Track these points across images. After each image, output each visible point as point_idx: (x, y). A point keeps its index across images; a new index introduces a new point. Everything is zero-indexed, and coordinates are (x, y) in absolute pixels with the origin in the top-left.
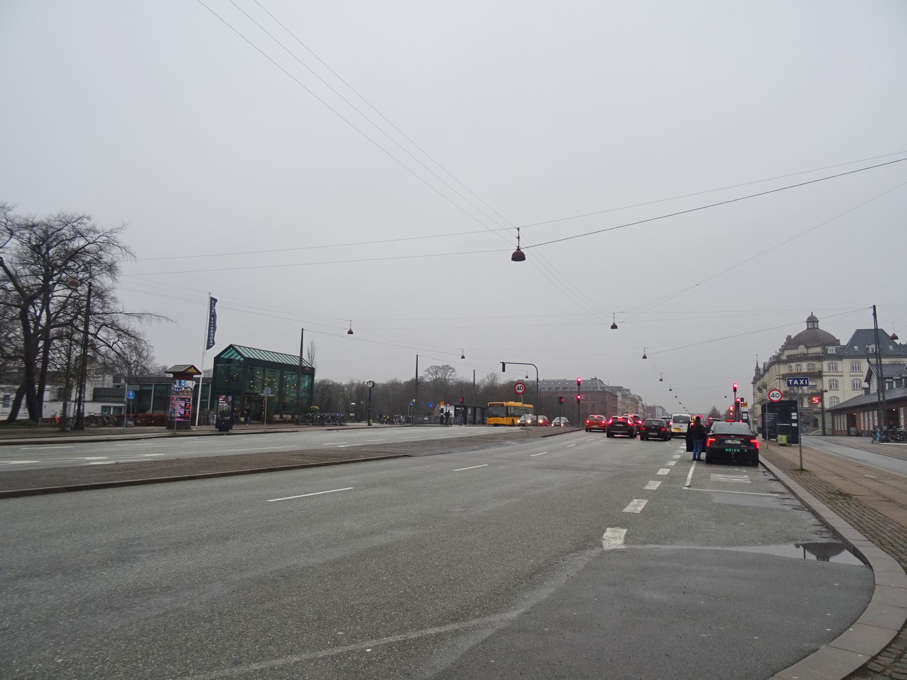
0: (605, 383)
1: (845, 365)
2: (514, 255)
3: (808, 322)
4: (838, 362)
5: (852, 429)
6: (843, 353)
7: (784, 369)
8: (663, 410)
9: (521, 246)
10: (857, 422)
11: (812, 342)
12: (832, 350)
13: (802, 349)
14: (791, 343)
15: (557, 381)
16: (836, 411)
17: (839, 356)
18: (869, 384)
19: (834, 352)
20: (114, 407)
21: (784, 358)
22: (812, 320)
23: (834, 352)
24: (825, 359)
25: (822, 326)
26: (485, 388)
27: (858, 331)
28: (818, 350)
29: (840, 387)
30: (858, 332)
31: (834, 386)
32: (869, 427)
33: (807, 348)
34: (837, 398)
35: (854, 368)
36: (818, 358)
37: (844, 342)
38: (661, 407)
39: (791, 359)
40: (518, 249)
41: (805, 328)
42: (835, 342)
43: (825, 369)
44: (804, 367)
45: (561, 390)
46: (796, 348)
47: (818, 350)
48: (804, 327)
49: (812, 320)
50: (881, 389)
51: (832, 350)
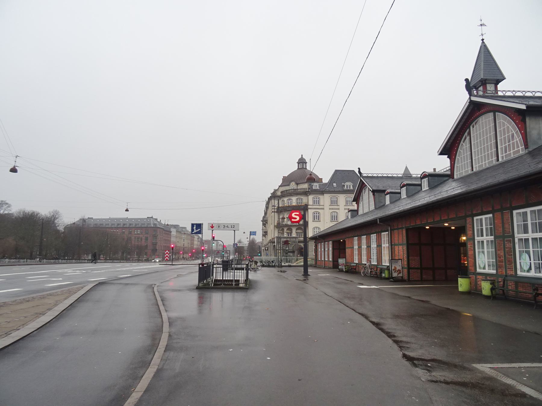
0: (163, 222)
1: (326, 199)
2: (299, 160)
3: (298, 163)
4: (321, 197)
5: (341, 261)
10: (348, 251)
11: (302, 180)
12: (316, 186)
13: (293, 186)
14: (286, 181)
15: (116, 219)
16: (321, 238)
17: (322, 192)
18: (358, 204)
19: (318, 188)
22: (302, 162)
23: (318, 188)
26: (65, 228)
27: (336, 171)
28: (305, 186)
29: (321, 219)
31: (317, 218)
32: (360, 259)
33: (297, 184)
34: (319, 228)
35: (334, 202)
36: (306, 193)
37: (326, 180)
39: (285, 194)
43: (311, 202)
44: (294, 201)
45: (104, 226)
46: (289, 185)
47: (305, 186)
48: (295, 167)
49: (302, 162)
50: (379, 206)
51: (316, 186)
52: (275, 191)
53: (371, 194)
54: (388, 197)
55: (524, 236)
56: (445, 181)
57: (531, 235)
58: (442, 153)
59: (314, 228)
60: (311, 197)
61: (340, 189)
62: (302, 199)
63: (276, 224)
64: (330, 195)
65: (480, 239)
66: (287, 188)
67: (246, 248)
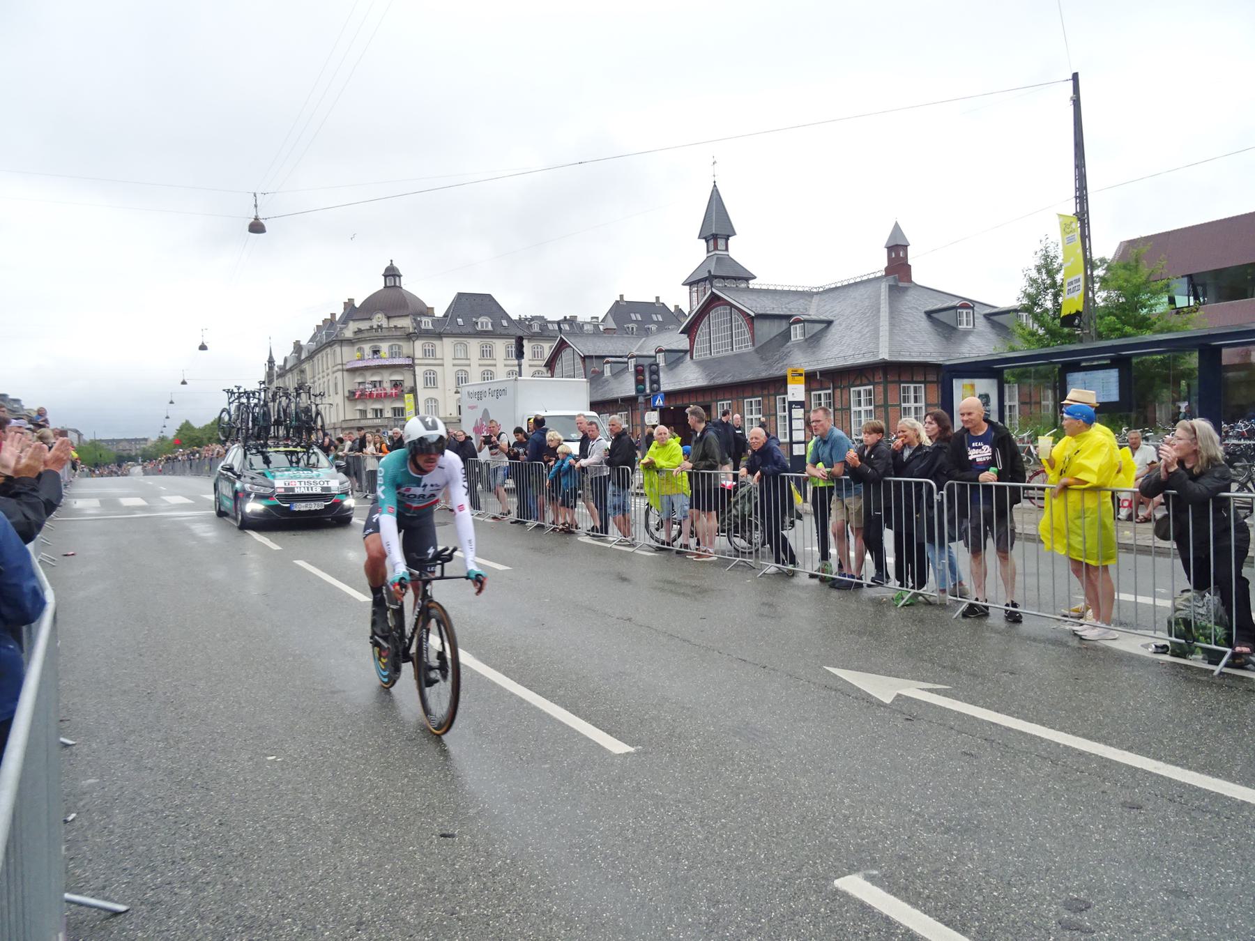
1: (446, 348)
2: (387, 270)
3: (386, 276)
4: (437, 343)
6: (442, 330)
7: (349, 356)
8: (80, 435)
9: (260, 216)
12: (485, 323)
19: (430, 327)
20: (916, 483)
21: (348, 333)
22: (391, 273)
23: (430, 327)
24: (417, 338)
25: (408, 284)
27: (460, 295)
28: (406, 323)
29: (440, 384)
30: (460, 296)
33: (389, 318)
36: (409, 337)
37: (439, 312)
38: (76, 431)
40: (256, 219)
41: (382, 286)
42: (428, 312)
43: (419, 353)
46: (370, 319)
47: (406, 323)
48: (379, 284)
49: (391, 273)
51: (426, 323)
52: (330, 323)
53: (578, 360)
54: (607, 368)
55: (858, 409)
56: (679, 359)
57: (754, 416)
58: (684, 284)
59: (427, 401)
60: (419, 344)
61: (470, 329)
62: (400, 347)
63: (347, 394)
64: (452, 340)
65: (858, 409)
66: (364, 325)
67: (949, 434)
